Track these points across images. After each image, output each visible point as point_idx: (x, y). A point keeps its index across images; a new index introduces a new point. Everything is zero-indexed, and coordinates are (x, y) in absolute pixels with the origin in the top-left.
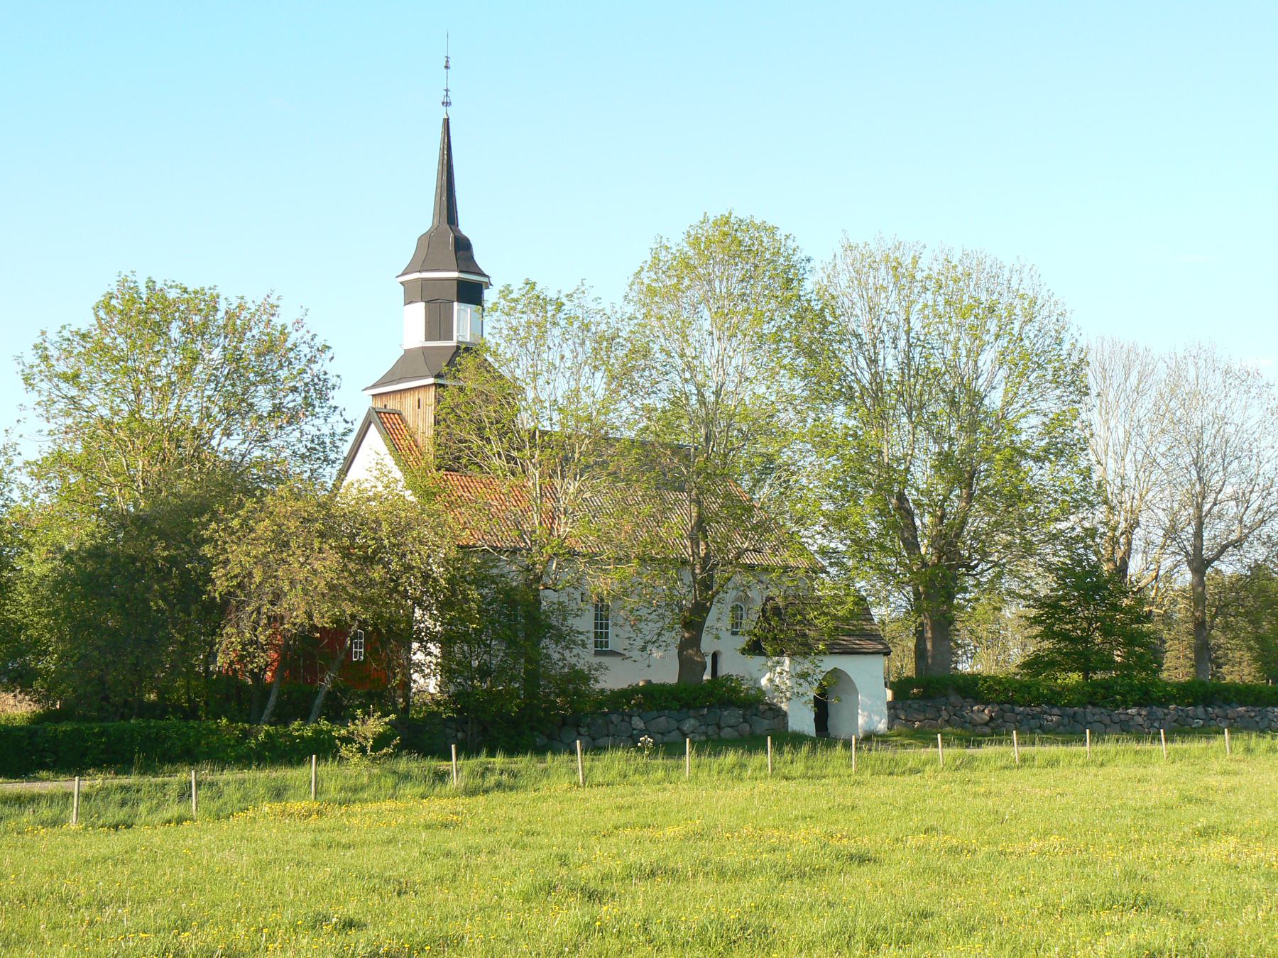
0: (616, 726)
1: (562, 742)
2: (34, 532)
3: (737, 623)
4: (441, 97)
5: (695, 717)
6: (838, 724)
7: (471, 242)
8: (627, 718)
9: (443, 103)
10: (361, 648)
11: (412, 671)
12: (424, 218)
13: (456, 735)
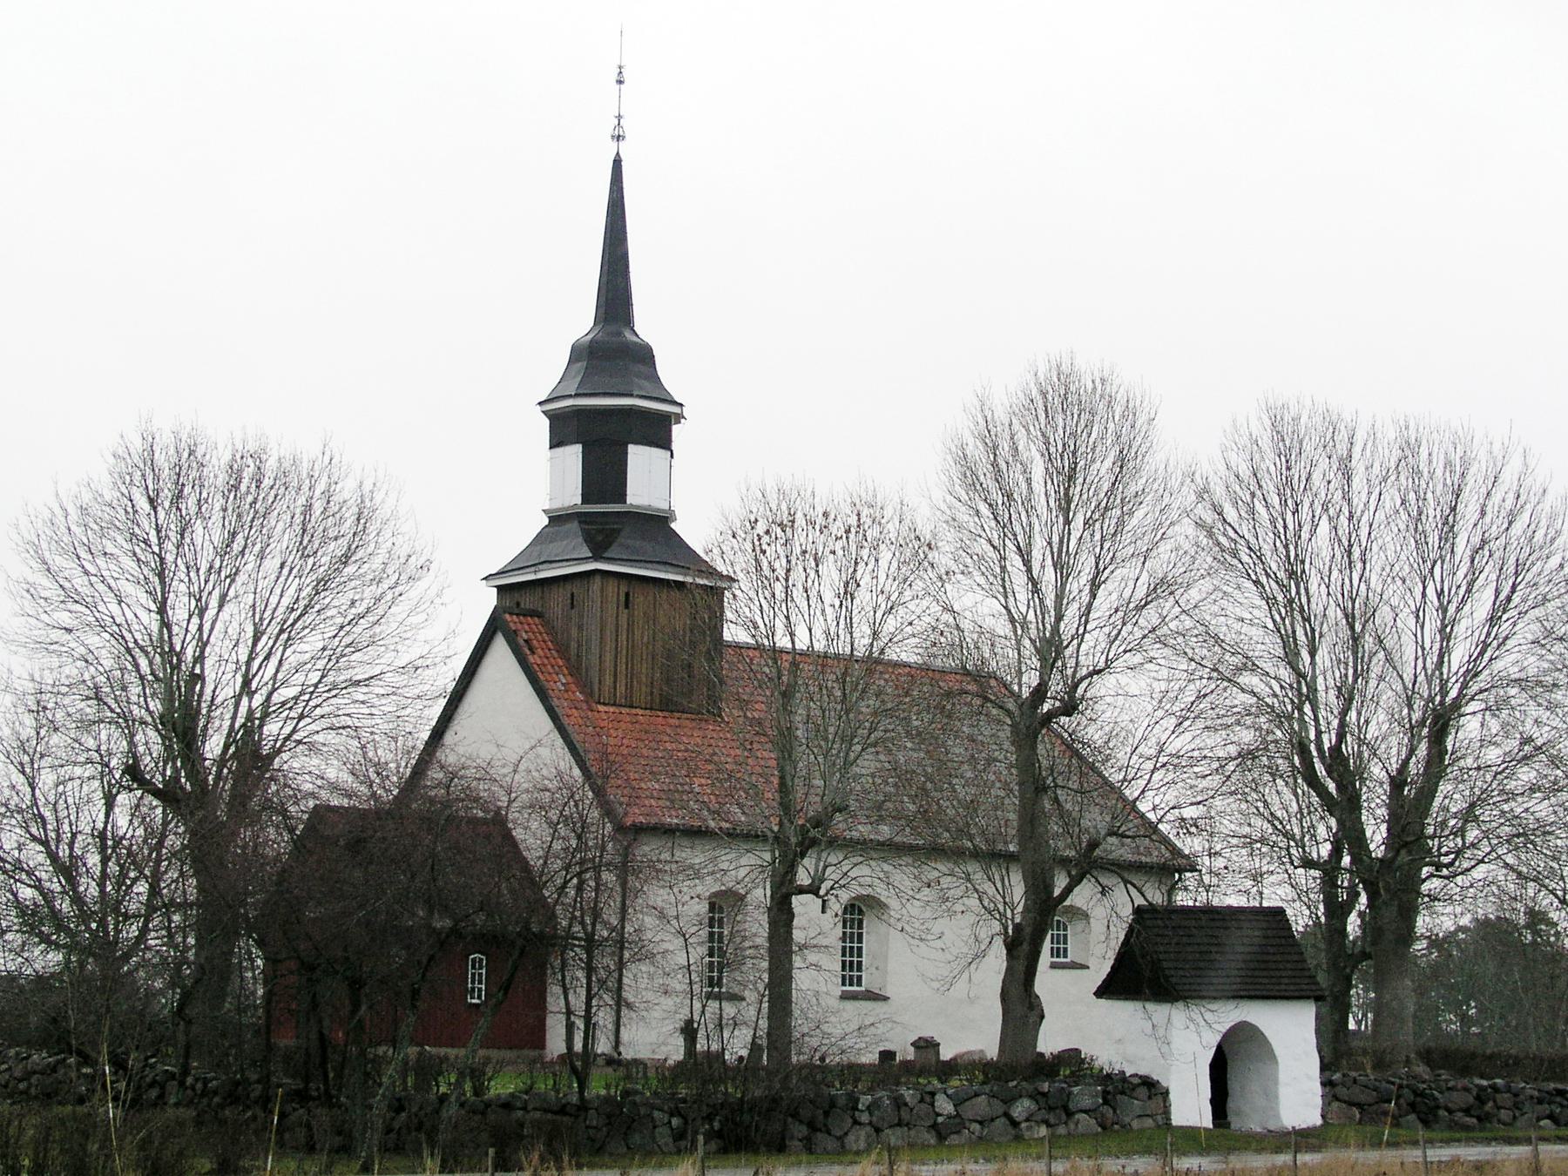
0: (912, 1110)
1: (830, 1134)
2: (571, 1128)
3: (1058, 949)
4: (615, 77)
5: (1031, 1097)
6: (1248, 1118)
7: (655, 353)
8: (928, 1098)
9: (613, 137)
10: (481, 968)
11: (1425, 871)
12: (581, 320)
13: (670, 1122)
